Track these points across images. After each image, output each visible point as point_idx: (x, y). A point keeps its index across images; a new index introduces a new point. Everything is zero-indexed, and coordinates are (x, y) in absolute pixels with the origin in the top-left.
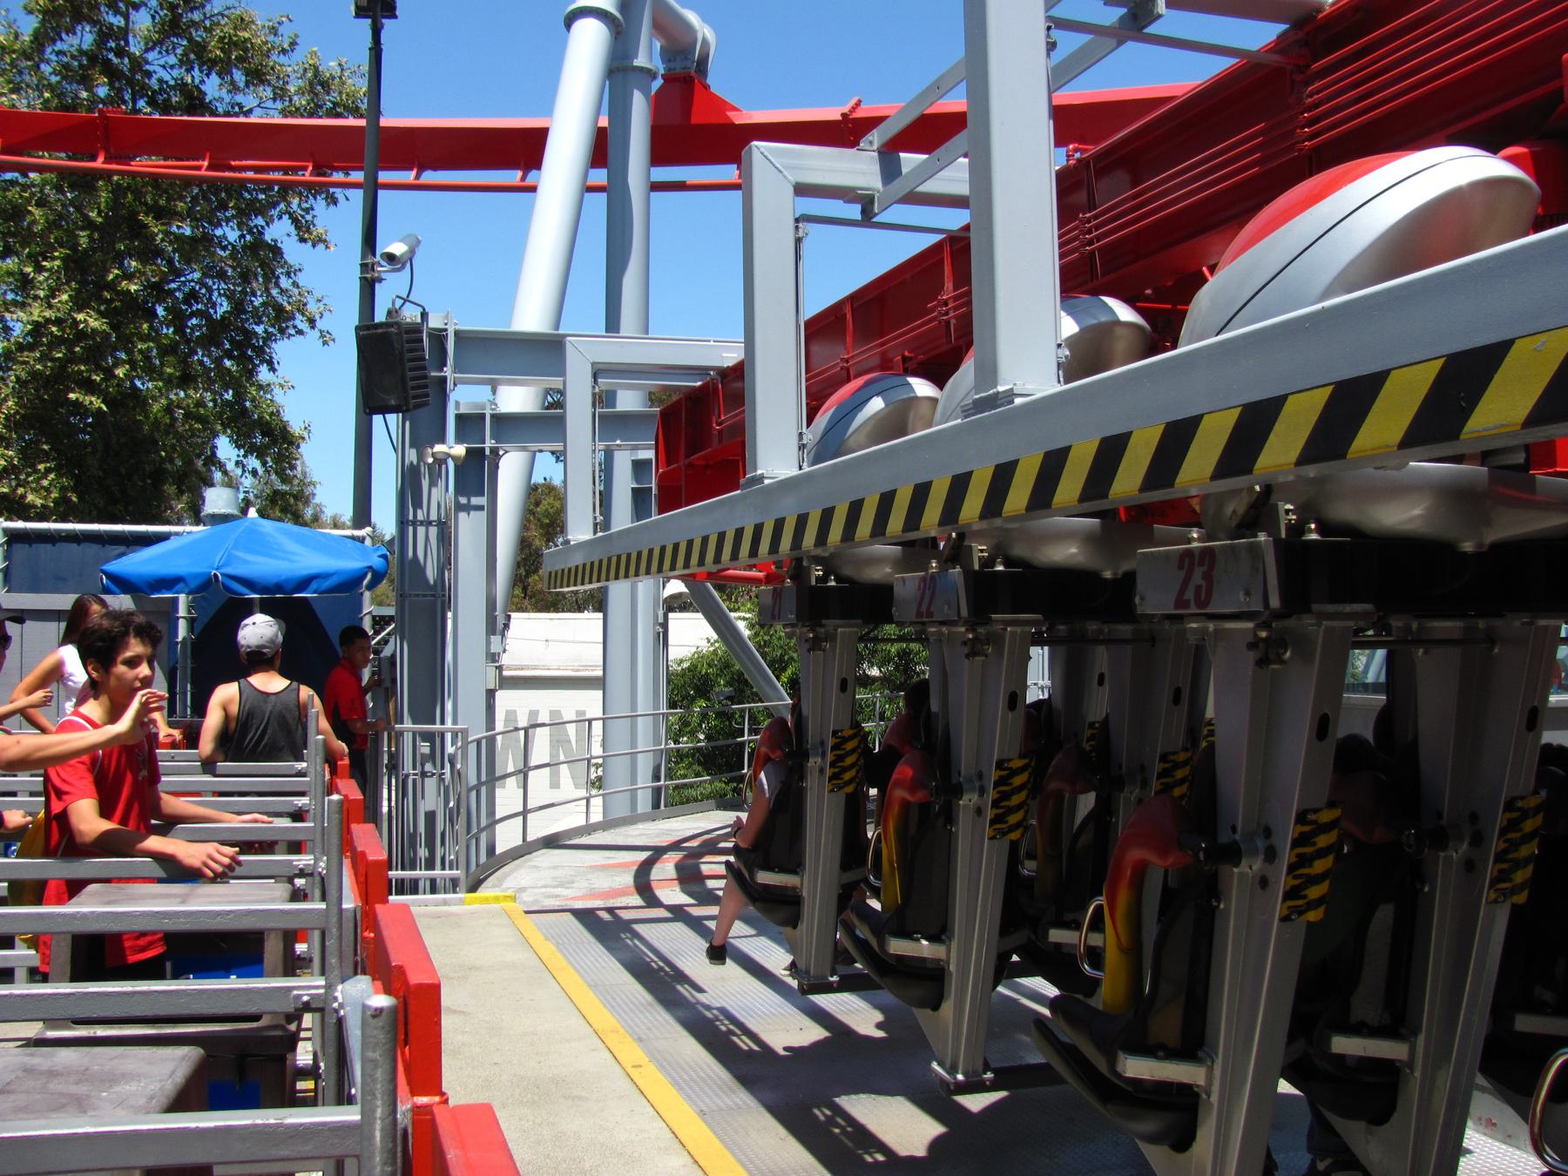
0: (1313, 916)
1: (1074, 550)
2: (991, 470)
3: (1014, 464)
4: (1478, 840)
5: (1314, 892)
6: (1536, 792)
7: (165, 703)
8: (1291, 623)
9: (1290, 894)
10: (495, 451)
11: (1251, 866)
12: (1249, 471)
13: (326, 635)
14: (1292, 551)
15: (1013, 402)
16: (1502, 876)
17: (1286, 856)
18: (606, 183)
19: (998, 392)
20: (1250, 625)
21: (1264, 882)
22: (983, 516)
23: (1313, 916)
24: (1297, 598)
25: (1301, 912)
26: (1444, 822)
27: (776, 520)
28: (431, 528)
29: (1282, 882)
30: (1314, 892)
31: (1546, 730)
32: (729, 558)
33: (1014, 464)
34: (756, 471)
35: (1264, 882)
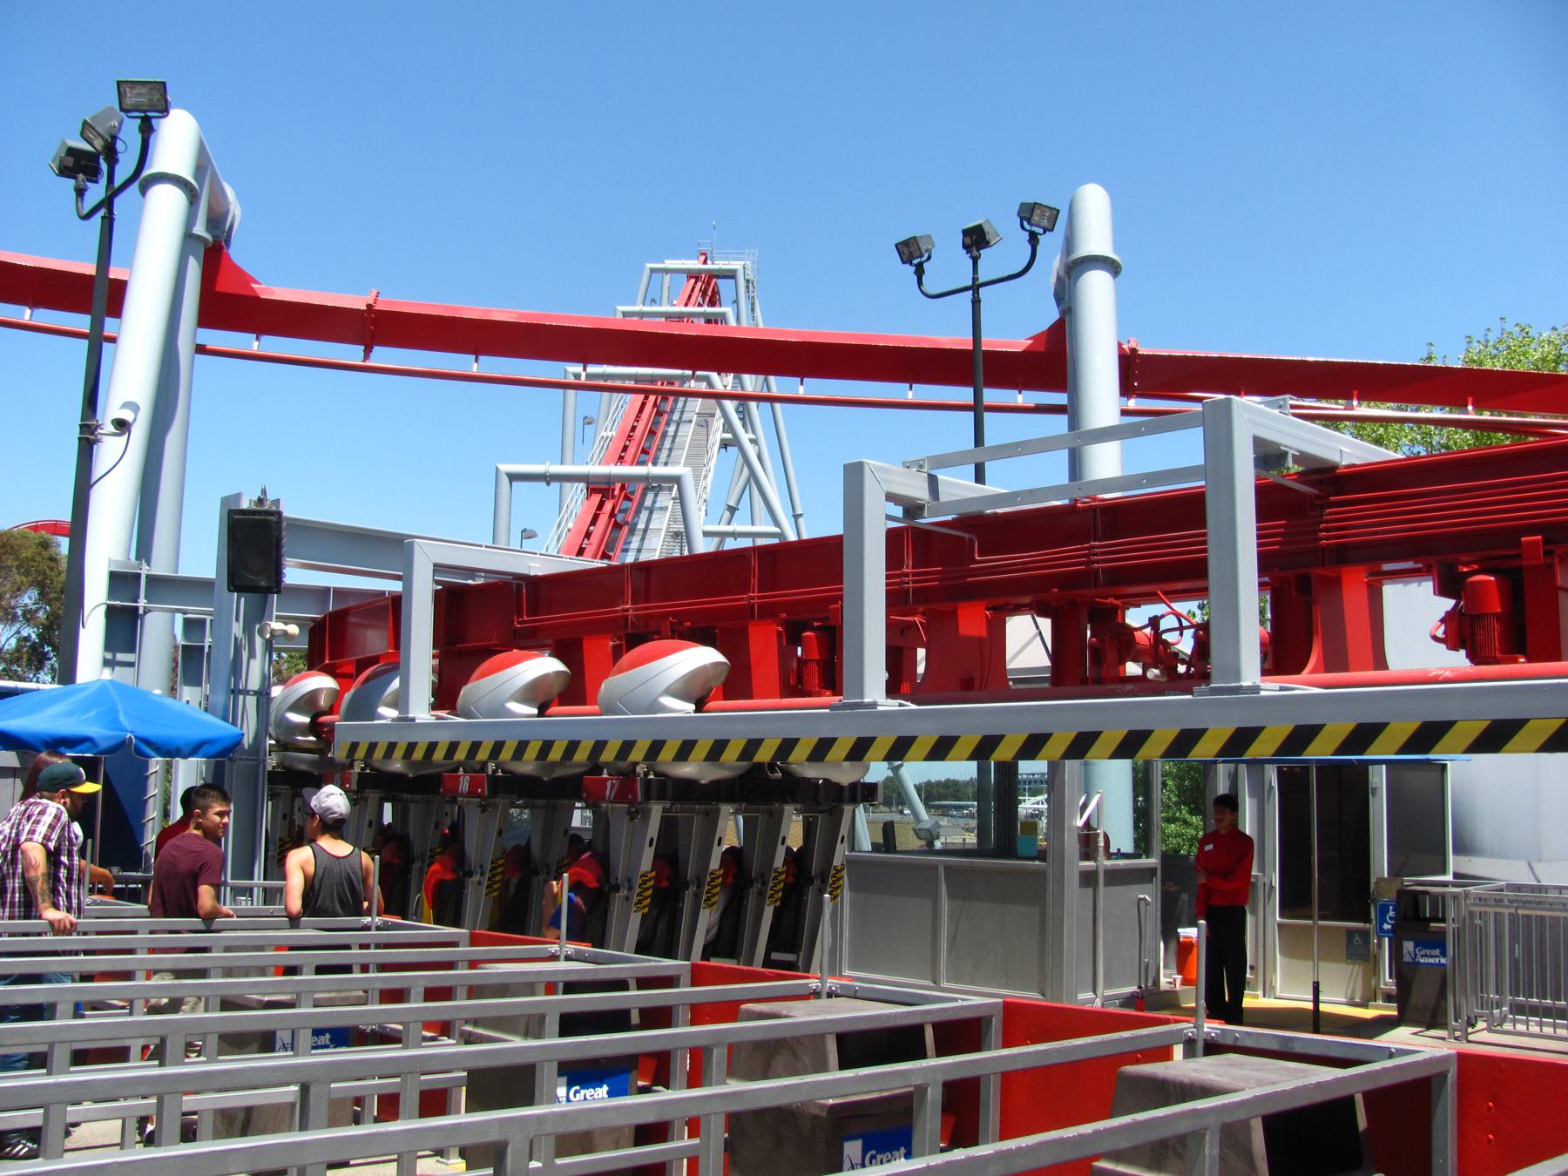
0: (495, 894)
1: (399, 766)
2: (936, 738)
3: (833, 740)
4: (631, 888)
5: (496, 886)
6: (567, 858)
7: (1430, 453)
8: (492, 800)
9: (488, 887)
10: (1296, 460)
11: (476, 878)
12: (626, 760)
13: (839, 831)
14: (493, 779)
15: (1259, 693)
16: (639, 902)
17: (488, 875)
18: (401, 590)
19: (863, 702)
20: (479, 800)
21: (480, 883)
22: (445, 758)
23: (495, 894)
24: (494, 791)
25: (491, 892)
26: (619, 881)
27: (370, 743)
28: (248, 697)
29: (486, 883)
30: (496, 886)
31: (17, 753)
32: (534, 755)
33: (833, 740)
34: (1239, 681)
35: (480, 883)
